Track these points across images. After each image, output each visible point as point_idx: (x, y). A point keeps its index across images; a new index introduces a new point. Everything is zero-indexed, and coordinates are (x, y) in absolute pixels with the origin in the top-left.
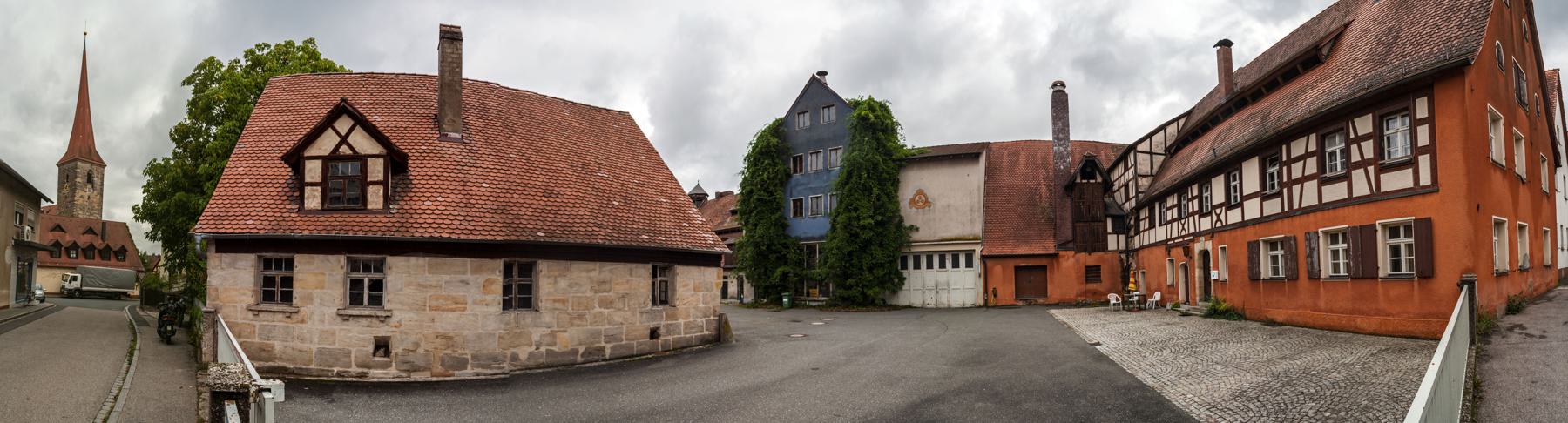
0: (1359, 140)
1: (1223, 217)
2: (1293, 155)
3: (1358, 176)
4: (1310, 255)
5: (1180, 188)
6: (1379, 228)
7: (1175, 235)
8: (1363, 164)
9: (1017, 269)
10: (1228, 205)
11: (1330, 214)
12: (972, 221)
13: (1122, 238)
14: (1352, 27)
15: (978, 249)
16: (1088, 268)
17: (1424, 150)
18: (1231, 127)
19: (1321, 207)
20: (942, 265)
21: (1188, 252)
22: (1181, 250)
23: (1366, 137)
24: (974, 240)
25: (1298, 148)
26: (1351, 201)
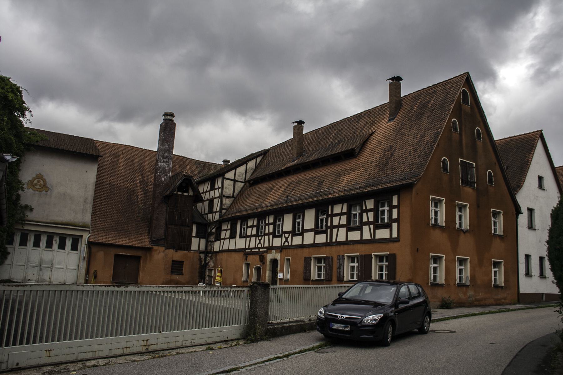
0: (367, 211)
1: (289, 240)
2: (335, 212)
3: (366, 228)
4: (339, 268)
5: (261, 216)
6: (373, 256)
7: (252, 246)
8: (368, 223)
9: (117, 256)
10: (294, 233)
11: (351, 247)
12: (84, 211)
13: (203, 241)
14: (373, 137)
15: (86, 236)
16: (174, 262)
17: (395, 221)
18: (299, 182)
19: (347, 243)
20: (49, 245)
21: (262, 259)
22: (257, 258)
23: (370, 210)
24: (83, 227)
25: (337, 209)
26: (361, 242)
